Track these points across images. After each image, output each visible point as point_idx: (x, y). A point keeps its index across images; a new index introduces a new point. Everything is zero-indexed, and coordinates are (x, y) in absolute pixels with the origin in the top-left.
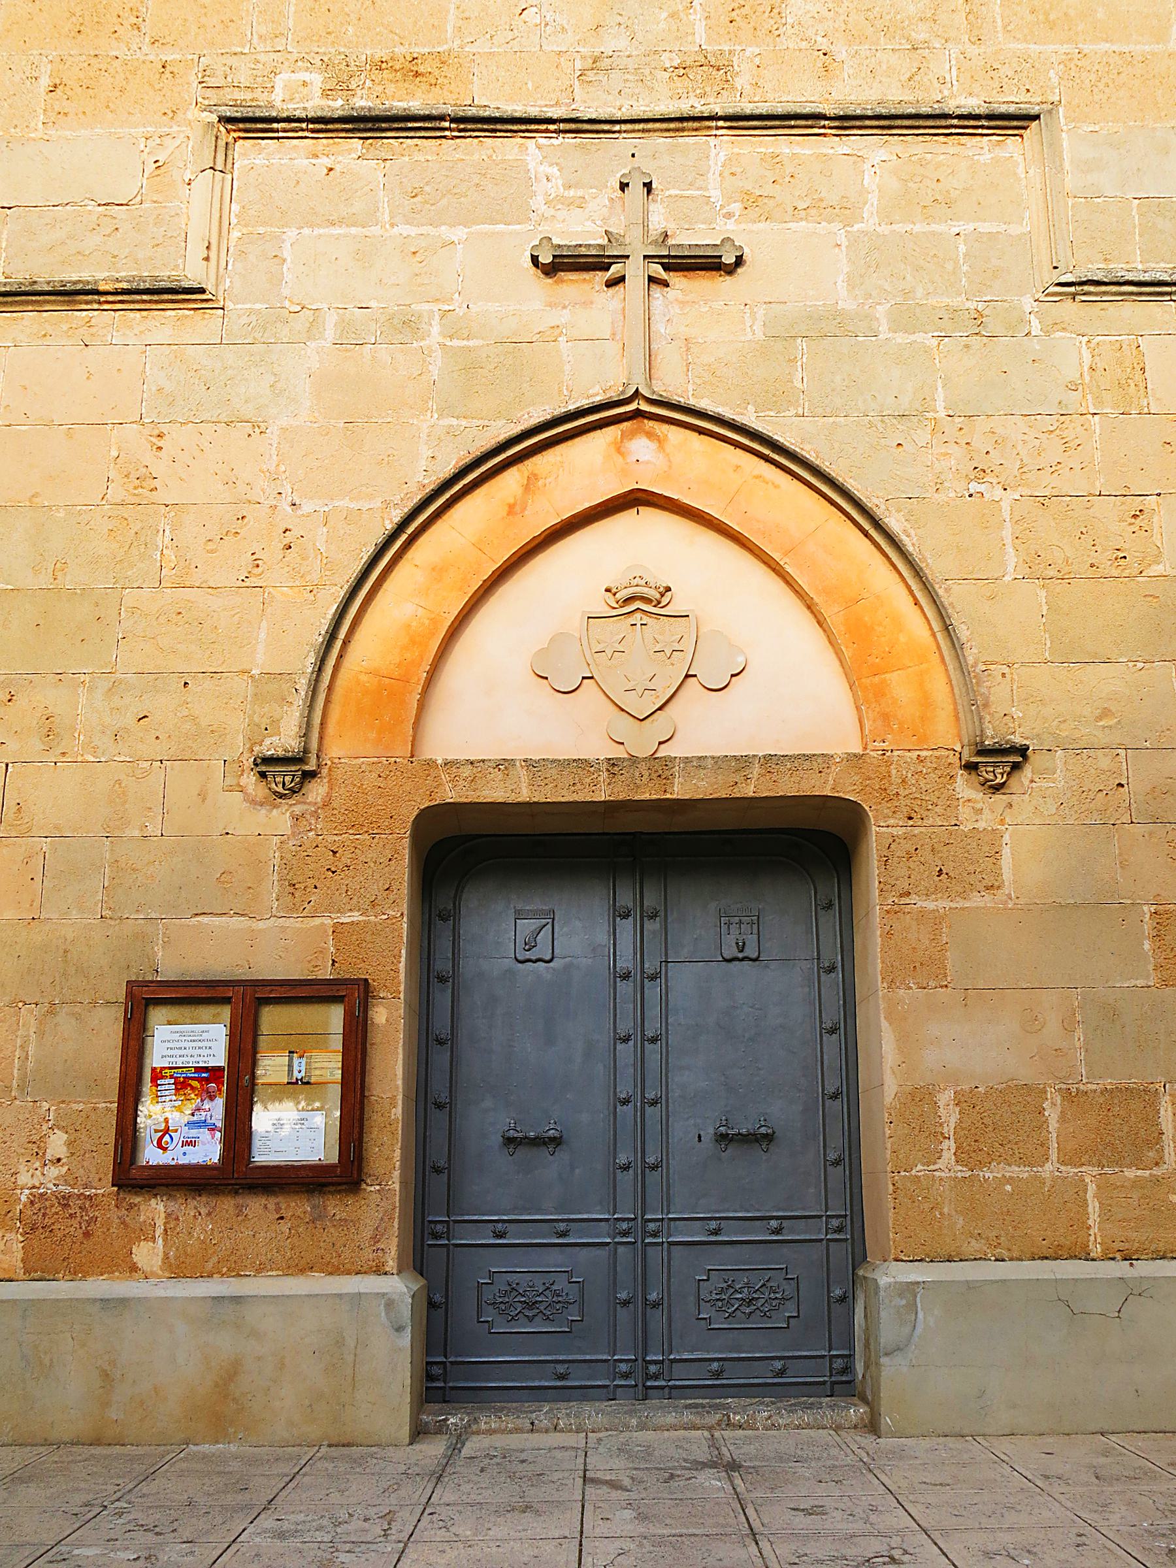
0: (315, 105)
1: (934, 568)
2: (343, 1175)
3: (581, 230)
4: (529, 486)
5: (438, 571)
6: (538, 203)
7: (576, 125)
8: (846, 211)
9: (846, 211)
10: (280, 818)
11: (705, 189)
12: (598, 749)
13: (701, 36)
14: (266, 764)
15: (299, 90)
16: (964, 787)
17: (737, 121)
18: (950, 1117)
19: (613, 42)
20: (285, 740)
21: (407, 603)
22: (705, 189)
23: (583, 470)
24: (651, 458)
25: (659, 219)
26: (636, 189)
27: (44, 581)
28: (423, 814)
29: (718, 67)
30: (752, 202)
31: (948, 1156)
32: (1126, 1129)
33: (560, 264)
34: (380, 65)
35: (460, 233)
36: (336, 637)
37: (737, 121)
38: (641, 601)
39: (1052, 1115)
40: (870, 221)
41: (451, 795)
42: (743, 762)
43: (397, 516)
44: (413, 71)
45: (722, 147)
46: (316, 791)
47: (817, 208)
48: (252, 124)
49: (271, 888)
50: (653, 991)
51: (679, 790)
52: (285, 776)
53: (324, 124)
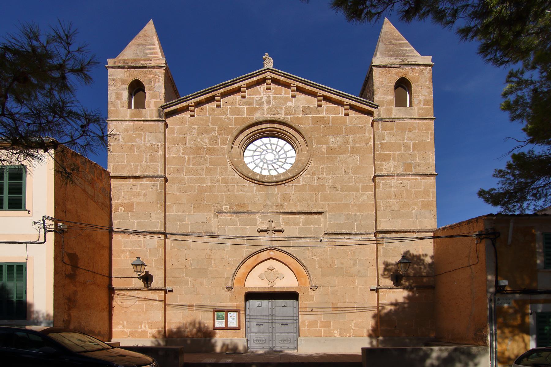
0: (228, 210)
1: (307, 266)
2: (238, 329)
3: (264, 227)
4: (258, 257)
5: (247, 266)
6: (258, 223)
7: (262, 213)
8: (298, 224)
9: (298, 224)
10: (229, 293)
11: (280, 222)
12: (267, 286)
13: (279, 201)
14: (227, 288)
15: (226, 208)
16: (310, 290)
17: (284, 213)
18: (307, 323)
19: (268, 202)
20: (229, 285)
21: (242, 270)
22: (280, 222)
23: (264, 255)
24: (272, 254)
25: (273, 225)
26: (271, 222)
27: (199, 267)
28: (422, 55)
29: (281, 206)
30: (286, 223)
31: (307, 327)
32: (261, 165)
33: (260, 231)
34: (237, 205)
35: (248, 227)
36: (235, 274)
37: (284, 213)
38: (271, 269)
39: (319, 323)
40: (301, 225)
41: (249, 290)
42: (284, 287)
43: (241, 260)
44: (241, 206)
45: (282, 216)
46: (233, 290)
47: (295, 224)
48: (221, 213)
49: (229, 300)
50: (274, 310)
51: (276, 290)
52: (229, 289)
53: (230, 213)
